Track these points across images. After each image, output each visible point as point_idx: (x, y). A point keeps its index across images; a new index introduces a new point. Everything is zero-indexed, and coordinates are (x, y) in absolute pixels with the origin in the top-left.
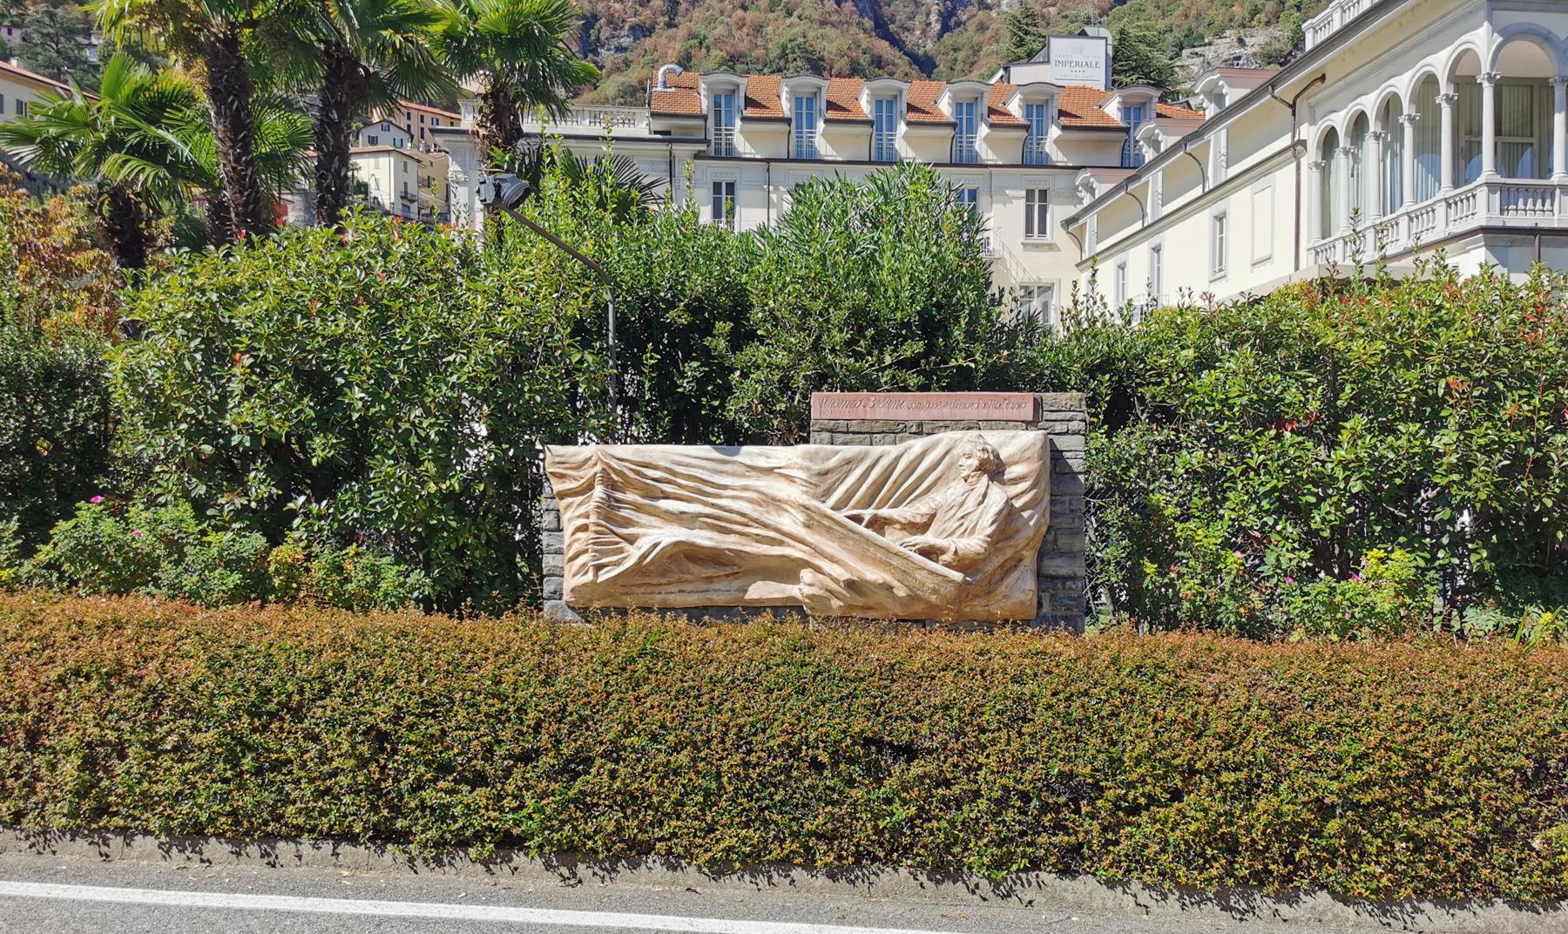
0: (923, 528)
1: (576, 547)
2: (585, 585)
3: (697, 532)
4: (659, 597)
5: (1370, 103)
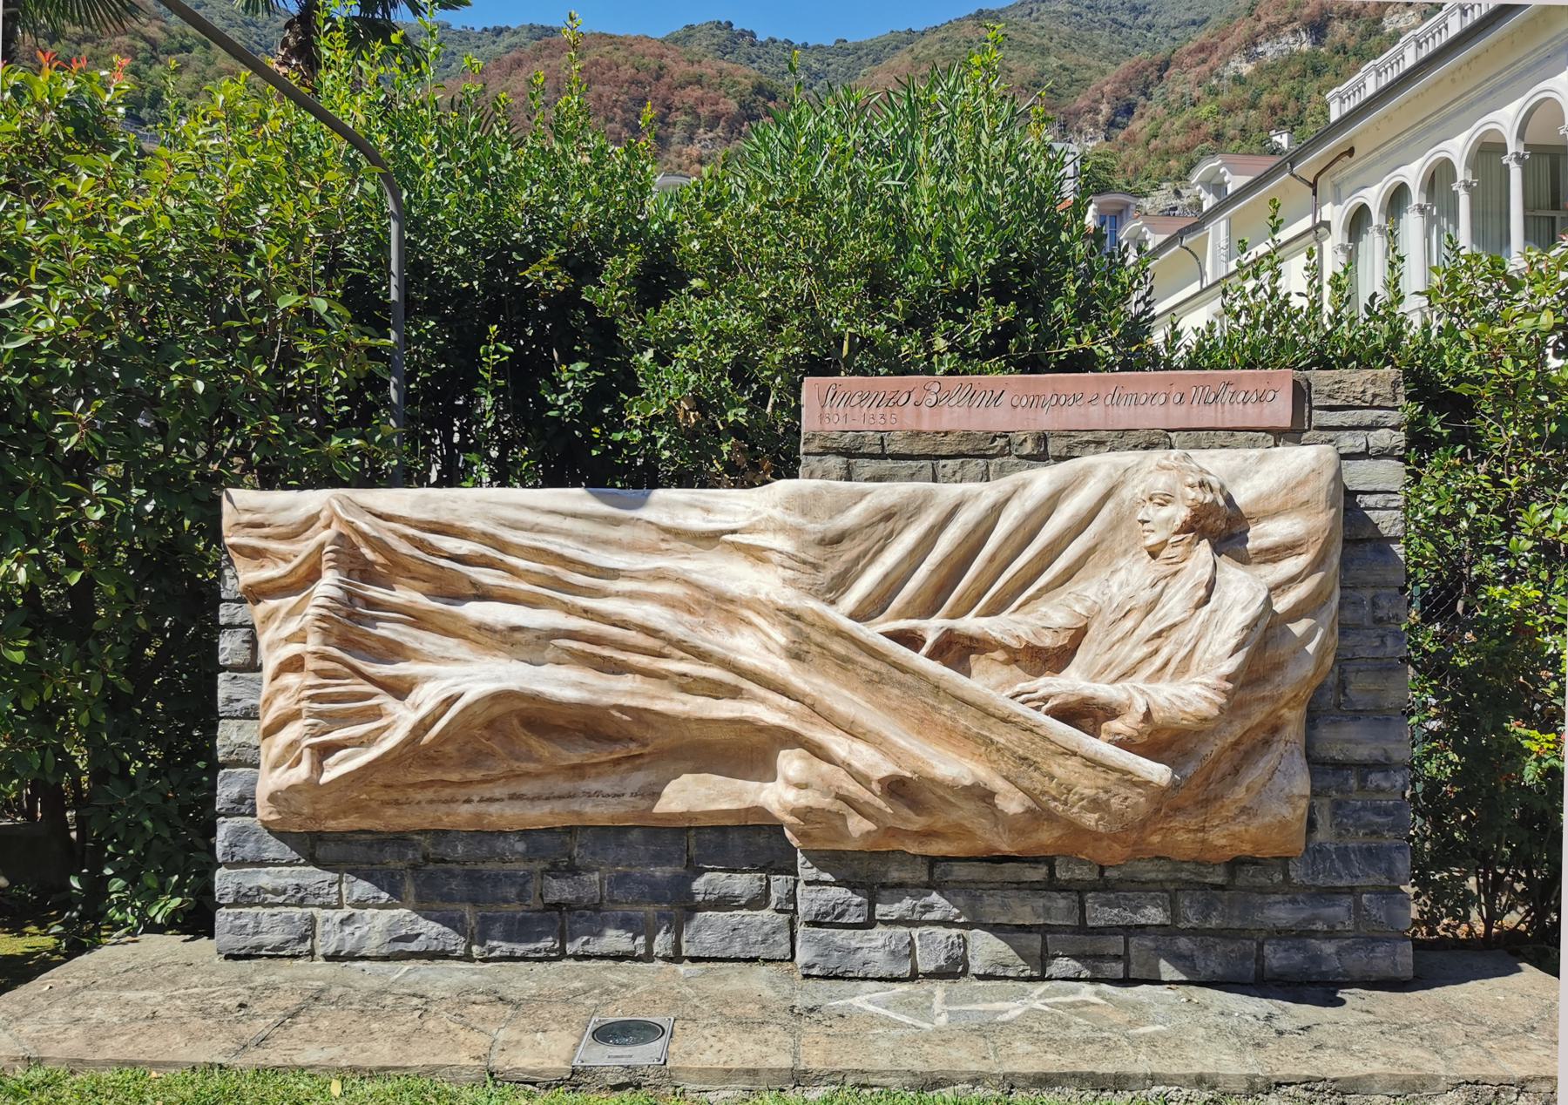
0: (1056, 659)
1: (281, 705)
2: (292, 788)
3: (548, 670)
4: (465, 810)
5: (1413, 174)
